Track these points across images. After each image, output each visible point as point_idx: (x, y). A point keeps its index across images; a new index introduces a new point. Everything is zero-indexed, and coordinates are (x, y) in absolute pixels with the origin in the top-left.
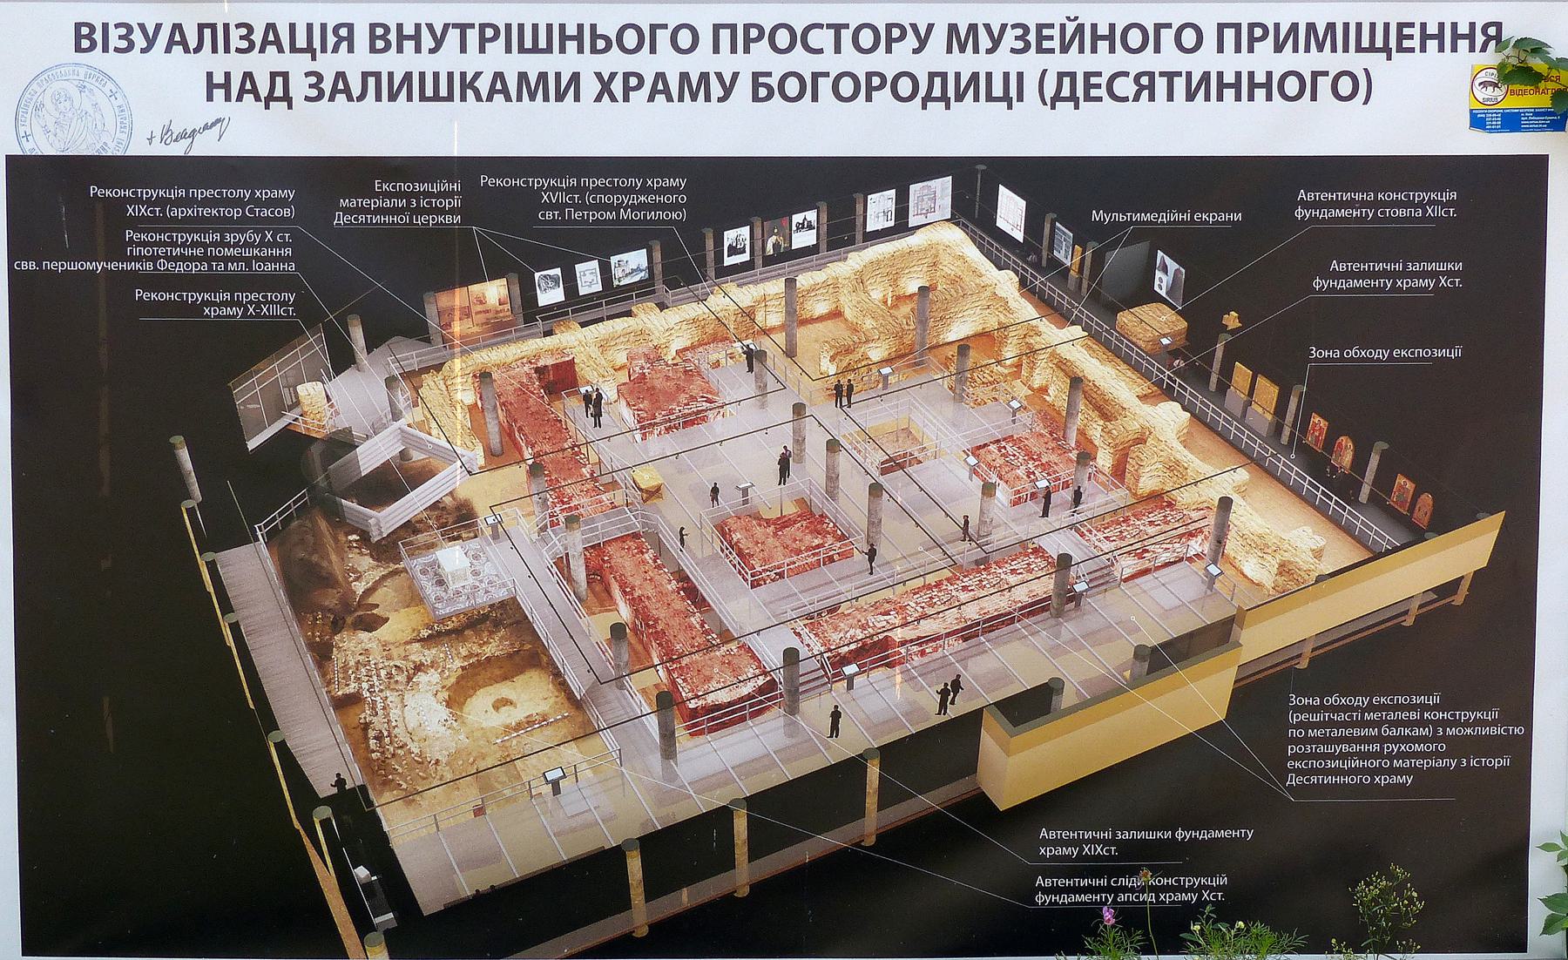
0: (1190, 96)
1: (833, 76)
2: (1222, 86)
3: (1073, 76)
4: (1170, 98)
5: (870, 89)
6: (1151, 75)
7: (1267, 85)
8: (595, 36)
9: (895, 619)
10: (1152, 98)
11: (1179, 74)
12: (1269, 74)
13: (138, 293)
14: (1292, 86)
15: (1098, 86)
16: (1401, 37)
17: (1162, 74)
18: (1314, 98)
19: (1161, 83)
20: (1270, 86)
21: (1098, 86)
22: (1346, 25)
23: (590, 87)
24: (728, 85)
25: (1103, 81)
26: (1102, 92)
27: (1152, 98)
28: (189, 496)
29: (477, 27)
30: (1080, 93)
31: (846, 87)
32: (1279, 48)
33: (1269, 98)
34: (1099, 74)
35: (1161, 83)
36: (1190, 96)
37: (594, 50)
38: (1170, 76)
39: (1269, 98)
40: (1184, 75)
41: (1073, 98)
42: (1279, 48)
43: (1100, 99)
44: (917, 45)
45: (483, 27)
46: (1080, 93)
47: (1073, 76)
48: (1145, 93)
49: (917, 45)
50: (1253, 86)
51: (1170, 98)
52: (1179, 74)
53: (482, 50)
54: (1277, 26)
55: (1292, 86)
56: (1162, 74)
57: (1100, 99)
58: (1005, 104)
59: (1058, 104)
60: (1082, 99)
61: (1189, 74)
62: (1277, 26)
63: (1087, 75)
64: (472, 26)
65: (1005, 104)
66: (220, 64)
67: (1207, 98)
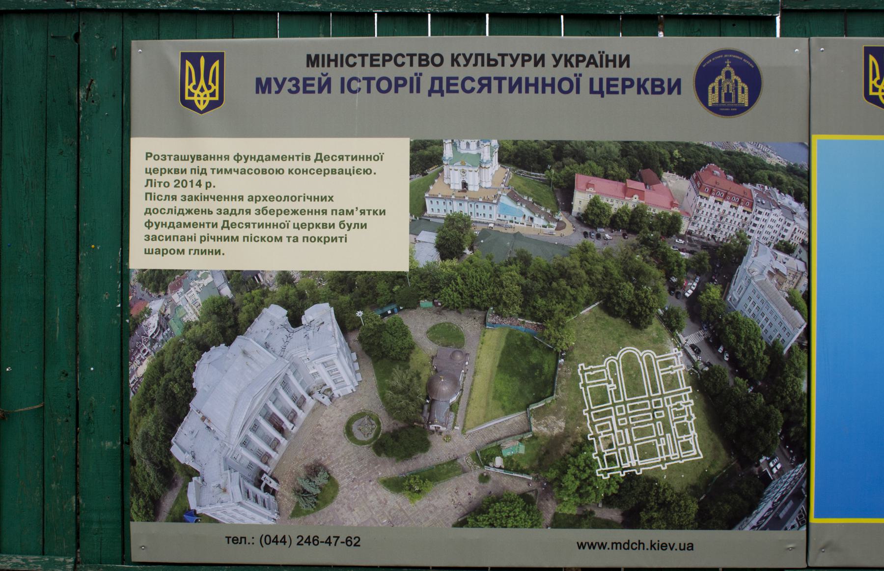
0: (511, 90)
1: (377, 79)
2: (528, 85)
3: (440, 79)
4: (500, 91)
5: (397, 86)
6: (489, 79)
7: (552, 85)
8: (489, 59)
9: (136, 510)
10: (489, 91)
11: (505, 78)
12: (553, 79)
13: (704, 66)
14: (566, 86)
15: (456, 85)
16: (609, 86)
17: (495, 78)
18: (578, 92)
19: (495, 84)
20: (553, 85)
21: (456, 85)
22: (323, 56)
23: (336, 85)
24: (322, 85)
25: (459, 82)
26: (459, 88)
27: (489, 91)
28: (660, 467)
29: (369, 55)
30: (444, 88)
31: (384, 85)
32: (536, 65)
33: (553, 92)
34: (457, 78)
35: (495, 84)
36: (511, 90)
37: (489, 65)
38: (500, 79)
39: (553, 92)
40: (508, 79)
41: (441, 91)
42: (536, 65)
43: (457, 92)
44: (555, 64)
45: (420, 55)
46: (444, 88)
47: (440, 79)
48: (486, 89)
49: (555, 64)
50: (544, 85)
51: (500, 91)
52: (505, 78)
53: (523, 65)
54: (535, 55)
55: (566, 86)
56: (495, 78)
57: (457, 92)
58: (600, 95)
59: (432, 94)
60: (445, 91)
61: (511, 79)
62: (535, 55)
63: (449, 79)
64: (415, 55)
65: (600, 95)
66: (621, 73)
67: (520, 91)
